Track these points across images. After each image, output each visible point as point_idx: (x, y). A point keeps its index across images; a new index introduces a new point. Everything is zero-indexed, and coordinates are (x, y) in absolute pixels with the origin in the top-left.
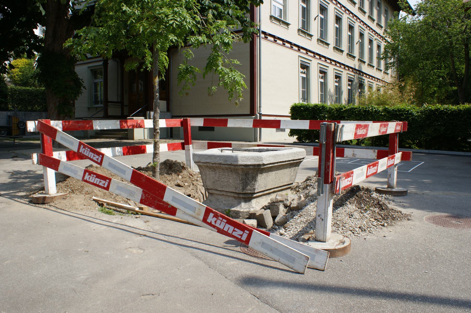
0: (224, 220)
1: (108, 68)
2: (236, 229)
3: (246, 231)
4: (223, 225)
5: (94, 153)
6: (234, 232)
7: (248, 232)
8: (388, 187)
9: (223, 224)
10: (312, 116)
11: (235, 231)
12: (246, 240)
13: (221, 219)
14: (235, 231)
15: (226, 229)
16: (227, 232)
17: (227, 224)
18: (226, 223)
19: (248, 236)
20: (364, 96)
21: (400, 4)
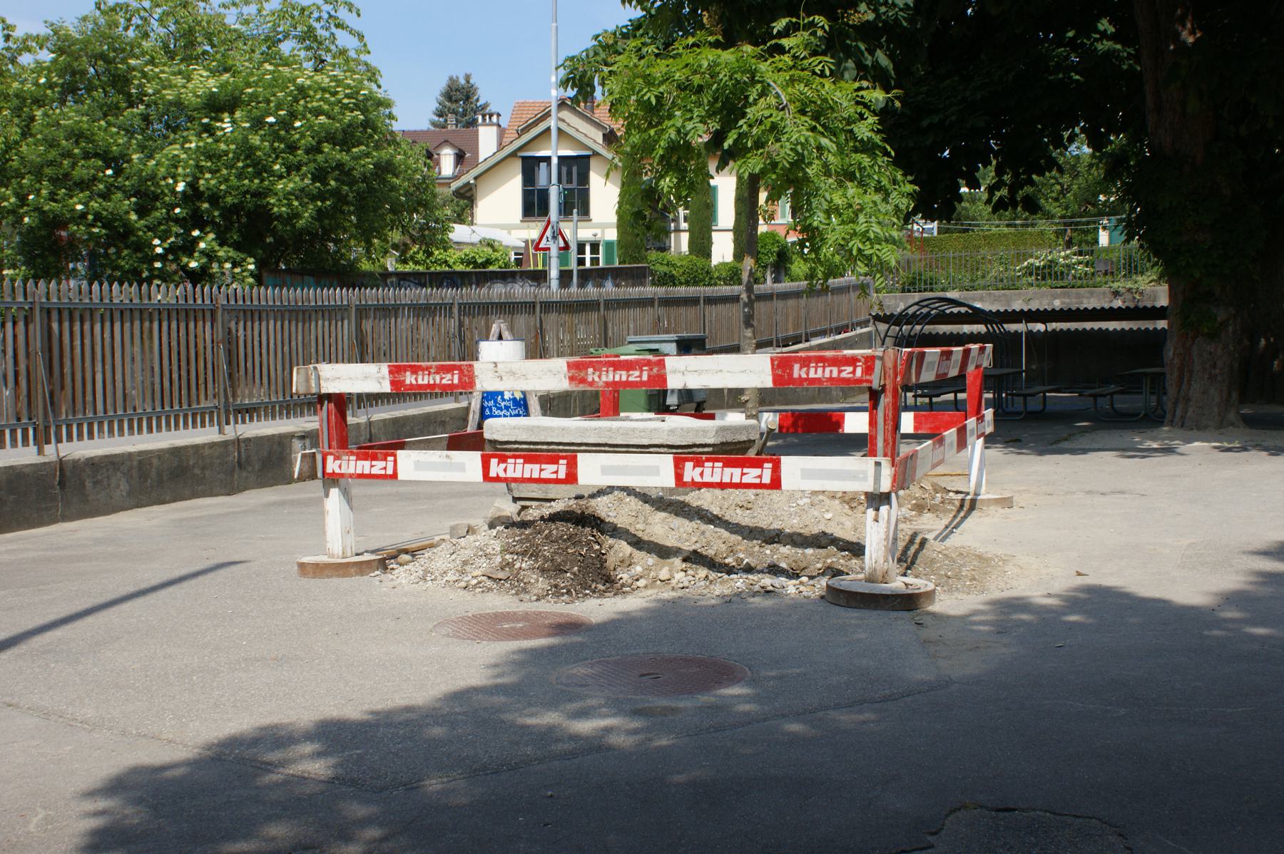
0: (717, 464)
1: (575, 154)
2: (745, 470)
3: (561, 461)
4: (953, 481)
5: (540, 463)
6: (760, 473)
7: (770, 465)
8: (474, 268)
9: (352, 463)
10: (671, 216)
11: (745, 474)
12: (772, 480)
13: (710, 464)
14: (745, 474)
15: (726, 480)
16: (523, 478)
17: (526, 465)
18: (723, 467)
19: (772, 472)
20: (209, 22)
21: (805, 58)
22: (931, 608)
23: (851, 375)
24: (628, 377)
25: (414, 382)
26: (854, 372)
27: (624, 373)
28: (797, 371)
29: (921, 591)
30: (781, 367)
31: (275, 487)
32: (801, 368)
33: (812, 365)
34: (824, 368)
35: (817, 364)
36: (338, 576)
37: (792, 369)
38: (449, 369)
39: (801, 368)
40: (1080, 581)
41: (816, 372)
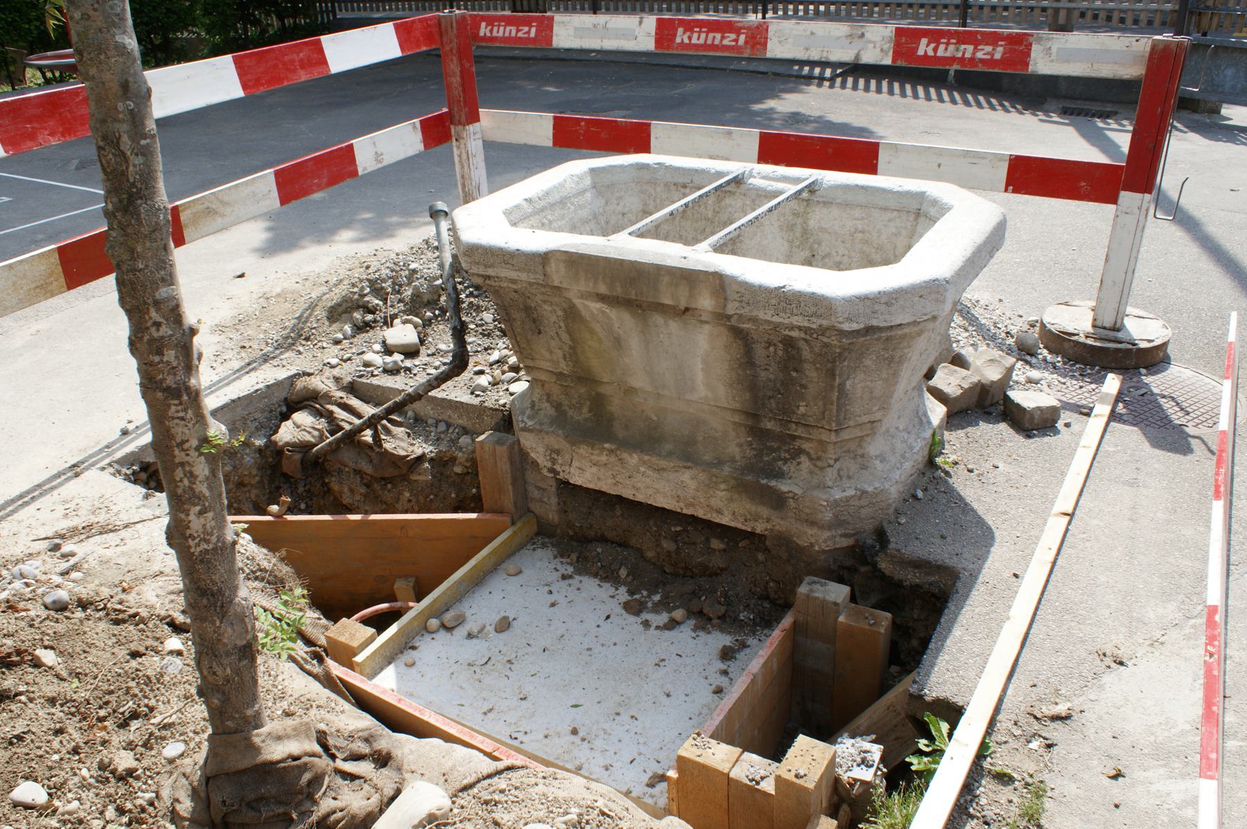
22: (1147, 380)
23: (734, 43)
24: (721, 40)
25: (686, 41)
26: (528, 32)
27: (514, 29)
28: (681, 36)
29: (1155, 344)
30: (664, 32)
31: (711, 270)
32: (684, 33)
33: (943, 41)
34: (707, 33)
35: (949, 40)
36: (946, 638)
37: (479, 27)
38: (528, 23)
39: (684, 33)
40: (694, 247)
41: (698, 39)
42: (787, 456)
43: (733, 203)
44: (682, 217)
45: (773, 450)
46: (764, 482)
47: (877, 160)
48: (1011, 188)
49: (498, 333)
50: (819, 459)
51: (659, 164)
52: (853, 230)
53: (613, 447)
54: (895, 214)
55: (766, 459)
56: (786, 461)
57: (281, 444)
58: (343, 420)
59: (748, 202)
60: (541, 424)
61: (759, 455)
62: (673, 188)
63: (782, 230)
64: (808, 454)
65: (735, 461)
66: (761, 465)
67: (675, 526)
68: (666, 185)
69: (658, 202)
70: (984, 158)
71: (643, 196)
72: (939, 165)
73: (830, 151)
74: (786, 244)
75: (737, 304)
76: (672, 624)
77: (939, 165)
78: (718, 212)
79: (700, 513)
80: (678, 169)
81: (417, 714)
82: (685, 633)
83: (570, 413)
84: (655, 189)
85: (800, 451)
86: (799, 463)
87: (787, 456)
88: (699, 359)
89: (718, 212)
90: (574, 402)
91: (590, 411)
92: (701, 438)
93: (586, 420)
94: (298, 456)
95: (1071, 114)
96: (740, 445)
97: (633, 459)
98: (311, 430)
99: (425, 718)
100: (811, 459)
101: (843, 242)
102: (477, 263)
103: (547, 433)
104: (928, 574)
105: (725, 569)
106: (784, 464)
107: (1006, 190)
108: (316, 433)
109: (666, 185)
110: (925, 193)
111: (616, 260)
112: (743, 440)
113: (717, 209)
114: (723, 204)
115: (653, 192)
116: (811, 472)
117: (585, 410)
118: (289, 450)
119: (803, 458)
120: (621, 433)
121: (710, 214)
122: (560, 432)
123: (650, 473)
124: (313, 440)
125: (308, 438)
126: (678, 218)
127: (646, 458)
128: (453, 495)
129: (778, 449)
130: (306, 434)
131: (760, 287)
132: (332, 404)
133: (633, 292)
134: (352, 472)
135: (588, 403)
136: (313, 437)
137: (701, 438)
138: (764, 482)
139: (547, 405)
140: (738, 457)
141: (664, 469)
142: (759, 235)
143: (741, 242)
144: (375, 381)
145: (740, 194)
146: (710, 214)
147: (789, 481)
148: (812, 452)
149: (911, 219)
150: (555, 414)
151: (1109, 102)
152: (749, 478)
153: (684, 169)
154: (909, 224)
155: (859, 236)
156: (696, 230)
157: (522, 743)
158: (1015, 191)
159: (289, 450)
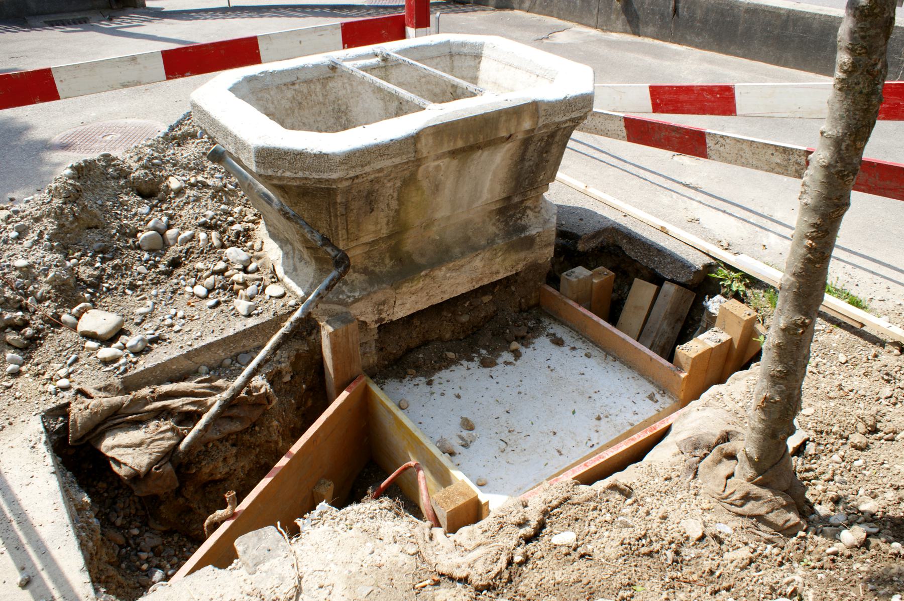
42: (520, 215)
43: (335, 84)
44: (299, 109)
45: (511, 216)
46: (523, 235)
47: (258, 50)
48: (346, 45)
49: (163, 277)
50: (536, 207)
51: (262, 73)
52: (418, 78)
53: (427, 271)
54: (438, 59)
55: (511, 224)
56: (521, 218)
57: (143, 469)
58: (183, 405)
59: (346, 81)
60: (365, 289)
61: (507, 223)
62: (284, 88)
63: (374, 93)
64: (529, 208)
65: (498, 235)
66: (511, 228)
67: (465, 303)
68: (278, 87)
69: (276, 102)
70: (326, 30)
71: (261, 102)
72: (300, 42)
73: (223, 52)
74: (381, 102)
75: (544, 118)
76: (517, 355)
77: (300, 42)
78: (326, 95)
79: (486, 282)
80: (282, 72)
81: (602, 460)
82: (527, 353)
83: (377, 270)
84: (269, 94)
85: (526, 208)
86: (528, 216)
87: (520, 215)
88: (491, 173)
89: (326, 95)
90: (376, 260)
91: (391, 259)
92: (471, 234)
93: (392, 267)
94: (169, 467)
95: (81, 23)
96: (494, 224)
97: (440, 273)
98: (162, 436)
99: (607, 457)
100: (532, 210)
101: (415, 88)
102: (354, 167)
103: (375, 292)
104: (599, 238)
105: (498, 309)
106: (521, 221)
107: (344, 48)
108: (169, 434)
109: (278, 87)
110: (449, 41)
111: (471, 117)
112: (494, 220)
113: (325, 93)
114: (328, 88)
115: (268, 96)
116: (536, 217)
117: (387, 261)
118: (157, 469)
119: (529, 212)
120: (422, 261)
121: (321, 99)
122: (384, 285)
123: (454, 274)
124: (172, 442)
125: (166, 444)
126: (296, 111)
127: (451, 265)
128: (293, 401)
129: (514, 215)
130: (159, 442)
131: (556, 101)
132: (151, 402)
133: (482, 137)
134: (218, 443)
135: (388, 255)
136: (169, 439)
137: (471, 234)
138: (523, 235)
139: (356, 275)
140: (497, 232)
141: (462, 266)
142: (360, 102)
143: (350, 111)
144: (140, 368)
145: (338, 76)
146: (321, 99)
147: (532, 228)
148: (531, 205)
149: (448, 59)
150: (367, 277)
151: (74, 11)
152: (515, 238)
153: (287, 71)
154: (448, 63)
155: (423, 80)
156: (314, 115)
157: (598, 443)
158: (349, 47)
159: (157, 469)
